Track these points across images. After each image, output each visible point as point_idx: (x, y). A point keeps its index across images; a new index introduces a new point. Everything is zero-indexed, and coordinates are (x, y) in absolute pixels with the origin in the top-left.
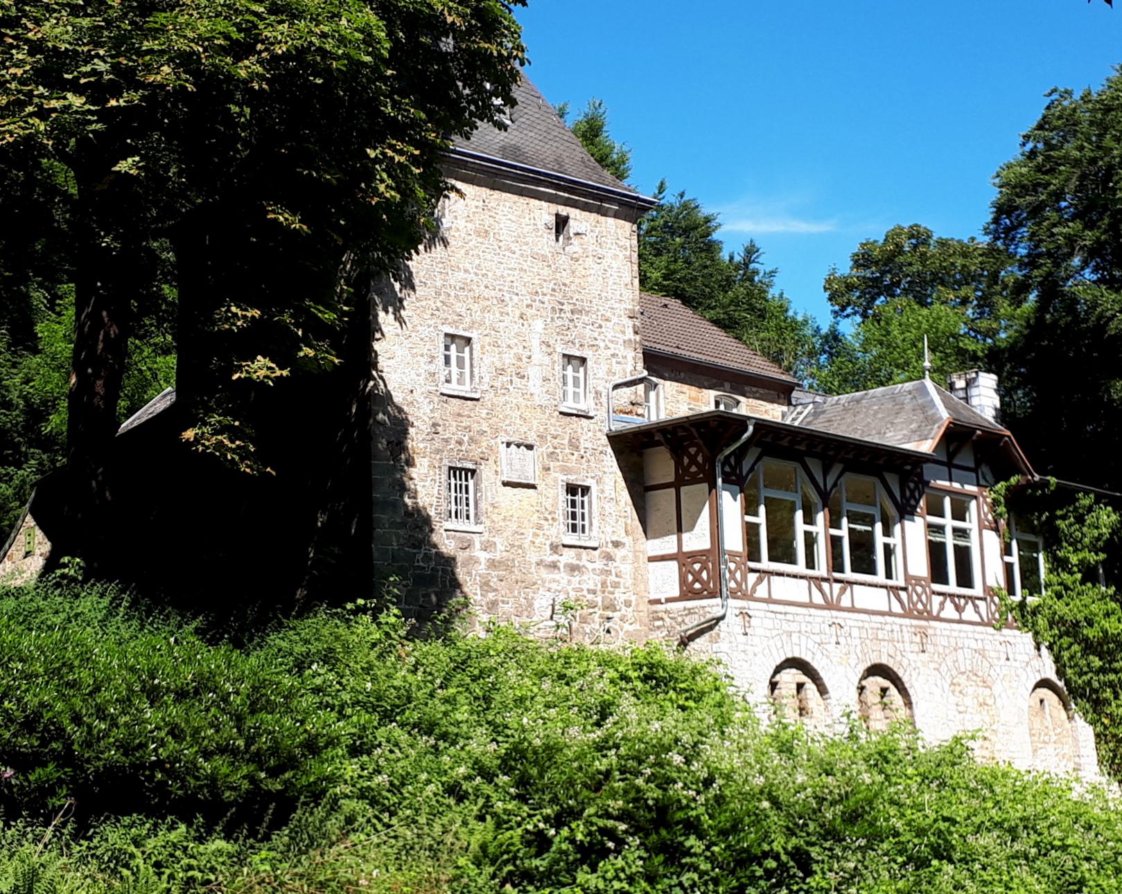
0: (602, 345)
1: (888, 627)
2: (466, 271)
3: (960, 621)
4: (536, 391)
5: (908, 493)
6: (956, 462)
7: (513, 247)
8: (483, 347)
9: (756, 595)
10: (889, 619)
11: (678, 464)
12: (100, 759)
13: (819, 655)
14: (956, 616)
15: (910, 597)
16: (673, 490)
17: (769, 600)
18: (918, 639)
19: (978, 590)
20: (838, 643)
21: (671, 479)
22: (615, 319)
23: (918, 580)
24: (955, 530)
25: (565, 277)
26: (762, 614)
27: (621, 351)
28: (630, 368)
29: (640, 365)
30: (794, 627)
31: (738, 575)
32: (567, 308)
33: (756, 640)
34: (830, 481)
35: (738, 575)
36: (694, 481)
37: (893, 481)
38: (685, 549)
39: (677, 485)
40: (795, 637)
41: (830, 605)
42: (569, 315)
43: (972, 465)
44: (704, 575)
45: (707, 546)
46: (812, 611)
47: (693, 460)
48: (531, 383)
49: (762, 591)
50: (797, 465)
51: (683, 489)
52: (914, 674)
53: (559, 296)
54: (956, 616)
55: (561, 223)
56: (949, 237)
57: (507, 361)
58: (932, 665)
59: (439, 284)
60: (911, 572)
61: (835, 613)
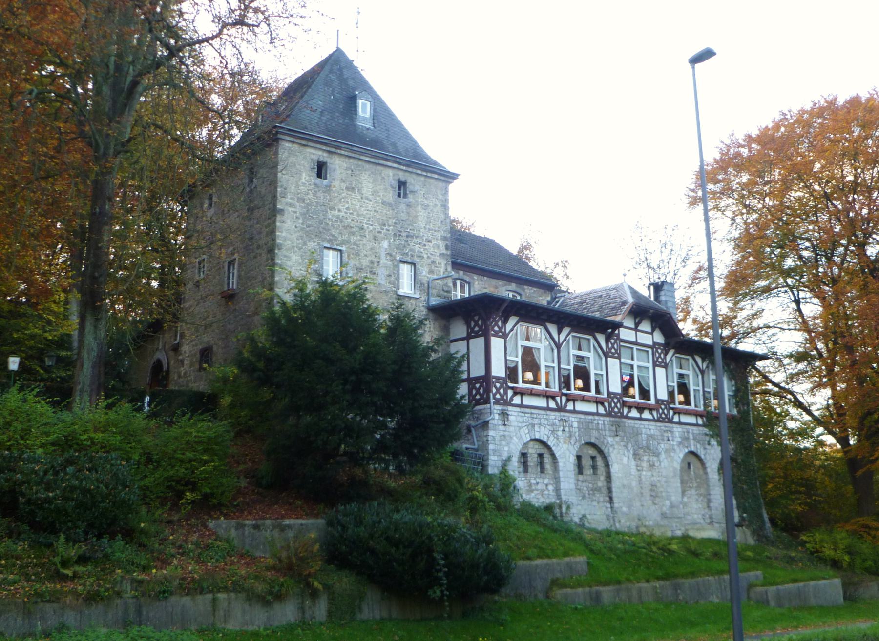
0: (425, 256)
1: (595, 422)
2: (339, 211)
3: (641, 419)
4: (383, 282)
5: (610, 346)
6: (639, 328)
7: (370, 197)
8: (348, 256)
9: (514, 402)
10: (596, 417)
11: (468, 326)
12: (786, 508)
13: (552, 438)
14: (638, 415)
15: (610, 405)
16: (465, 342)
17: (521, 406)
18: (614, 428)
19: (652, 401)
20: (564, 430)
21: (465, 335)
22: (434, 242)
23: (663, 401)
24: (638, 367)
25: (403, 216)
26: (516, 414)
27: (438, 260)
28: (442, 270)
29: (449, 268)
30: (536, 421)
31: (502, 391)
32: (404, 234)
33: (512, 429)
34: (563, 336)
35: (502, 391)
36: (477, 336)
37: (601, 338)
38: (472, 376)
39: (468, 338)
40: (537, 428)
41: (560, 409)
42: (405, 238)
43: (649, 330)
44: (481, 391)
45: (483, 373)
46: (548, 412)
47: (476, 324)
48: (379, 277)
49: (676, 419)
50: (541, 327)
51: (471, 341)
52: (611, 449)
53: (399, 227)
54: (638, 415)
55: (402, 184)
56: (429, 132)
57: (364, 264)
58: (622, 444)
59: (322, 217)
60: (611, 390)
61: (562, 414)
